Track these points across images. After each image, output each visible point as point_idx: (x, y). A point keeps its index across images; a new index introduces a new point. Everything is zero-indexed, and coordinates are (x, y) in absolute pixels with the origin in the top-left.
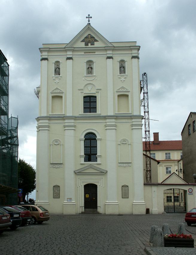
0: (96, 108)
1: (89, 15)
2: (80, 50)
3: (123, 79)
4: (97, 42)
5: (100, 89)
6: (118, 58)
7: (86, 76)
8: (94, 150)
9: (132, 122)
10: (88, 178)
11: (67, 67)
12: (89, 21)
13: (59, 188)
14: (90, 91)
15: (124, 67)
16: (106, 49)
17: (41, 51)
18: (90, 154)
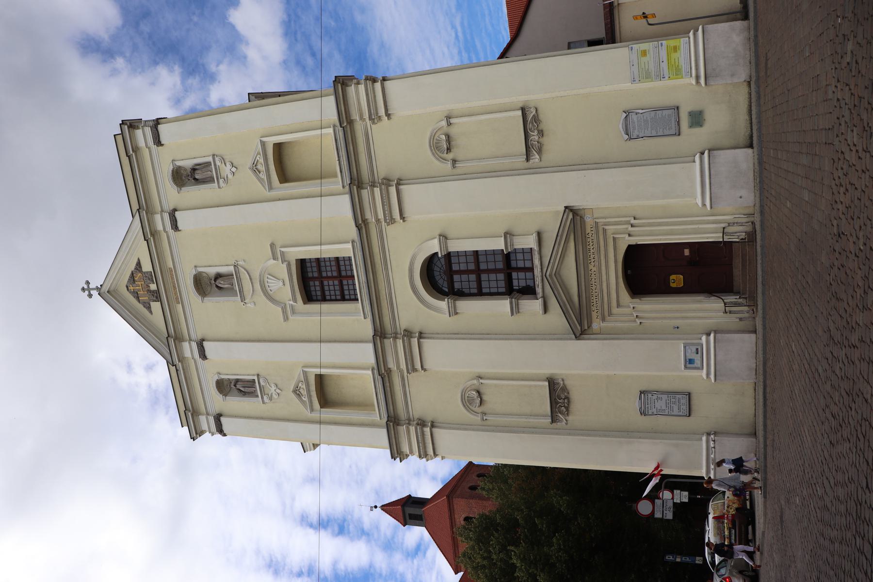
0: (337, 259)
2: (170, 317)
3: (226, 170)
5: (272, 246)
6: (168, 194)
7: (243, 299)
9: (378, 221)
11: (227, 359)
14: (284, 286)
16: (152, 235)
17: (200, 433)
18: (502, 274)
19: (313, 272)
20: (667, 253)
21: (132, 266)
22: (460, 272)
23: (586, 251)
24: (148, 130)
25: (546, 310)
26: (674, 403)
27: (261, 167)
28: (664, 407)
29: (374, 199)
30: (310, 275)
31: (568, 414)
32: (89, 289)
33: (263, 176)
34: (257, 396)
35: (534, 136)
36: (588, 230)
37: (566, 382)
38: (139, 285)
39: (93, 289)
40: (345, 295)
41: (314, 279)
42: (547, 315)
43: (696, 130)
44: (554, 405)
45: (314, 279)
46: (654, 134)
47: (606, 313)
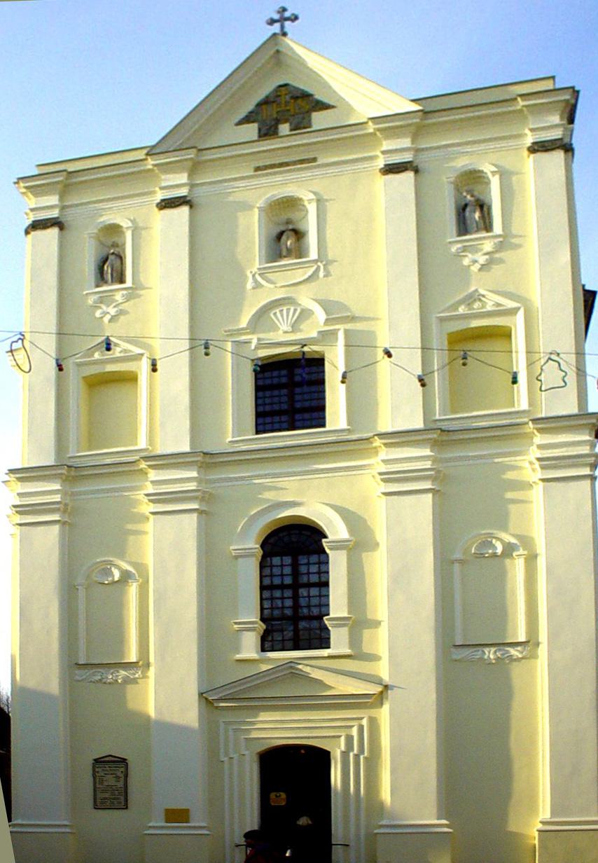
4: (329, 111)
8: (315, 601)
10: (324, 720)
13: (123, 769)
15: (481, 207)
24: (556, 134)
26: (113, 794)
28: (106, 783)
32: (282, 20)
34: (97, 286)
39: (282, 27)
40: (267, 419)
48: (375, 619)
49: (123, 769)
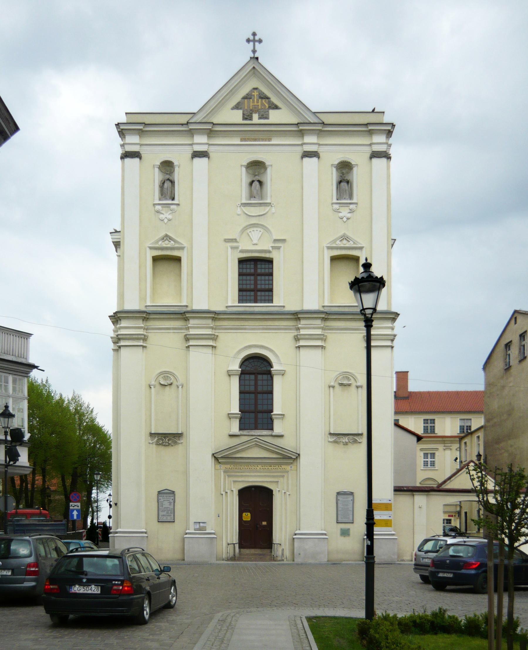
1: (254, 34)
11: (195, 179)
12: (254, 51)
14: (255, 244)
17: (122, 133)
19: (262, 269)
20: (267, 513)
21: (275, 100)
22: (256, 380)
23: (270, 464)
25: (231, 436)
26: (167, 513)
27: (345, 243)
28: (164, 506)
29: (314, 328)
30: (259, 266)
31: (157, 444)
33: (339, 243)
35: (345, 439)
36: (283, 467)
37: (180, 445)
38: (255, 102)
41: (256, 268)
42: (228, 436)
43: (339, 532)
44: (164, 436)
45: (256, 268)
46: (339, 509)
47: (229, 474)
48: (515, 596)
49: (173, 498)
